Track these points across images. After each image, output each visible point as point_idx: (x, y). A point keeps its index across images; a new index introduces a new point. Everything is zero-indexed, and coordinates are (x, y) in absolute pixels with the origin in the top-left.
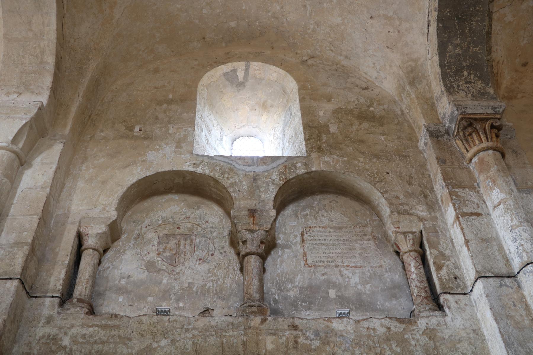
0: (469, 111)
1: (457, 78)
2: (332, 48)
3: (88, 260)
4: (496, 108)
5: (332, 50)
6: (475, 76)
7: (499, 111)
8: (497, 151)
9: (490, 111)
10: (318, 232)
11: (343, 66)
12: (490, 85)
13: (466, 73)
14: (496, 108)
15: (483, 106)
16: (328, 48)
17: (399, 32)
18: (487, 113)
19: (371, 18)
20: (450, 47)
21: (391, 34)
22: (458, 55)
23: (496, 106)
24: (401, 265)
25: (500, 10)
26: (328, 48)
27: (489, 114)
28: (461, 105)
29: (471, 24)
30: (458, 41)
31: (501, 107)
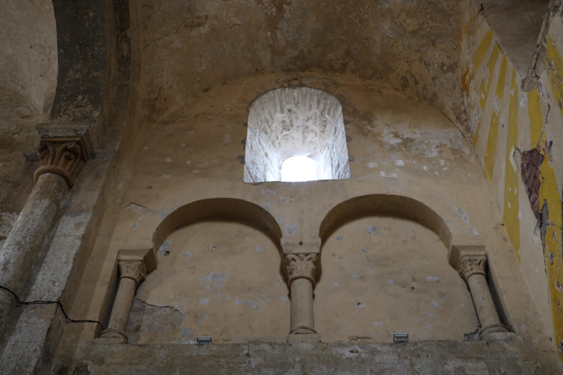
0: (51, 134)
1: (69, 102)
2: (12, 79)
3: (126, 286)
4: (78, 131)
5: (12, 81)
6: (89, 100)
7: (80, 134)
8: (56, 173)
9: (71, 134)
10: (479, 255)
11: (21, 96)
12: (99, 108)
13: (80, 97)
14: (78, 131)
15: (64, 129)
16: (9, 79)
17: (49, 60)
18: (68, 136)
19: (31, 47)
20: (71, 72)
21: (44, 62)
22: (78, 80)
23: (78, 129)
24: (466, 286)
25: (165, 37)
26: (9, 79)
27: (69, 137)
28: (42, 129)
29: (93, 49)
30: (79, 66)
31: (83, 130)
